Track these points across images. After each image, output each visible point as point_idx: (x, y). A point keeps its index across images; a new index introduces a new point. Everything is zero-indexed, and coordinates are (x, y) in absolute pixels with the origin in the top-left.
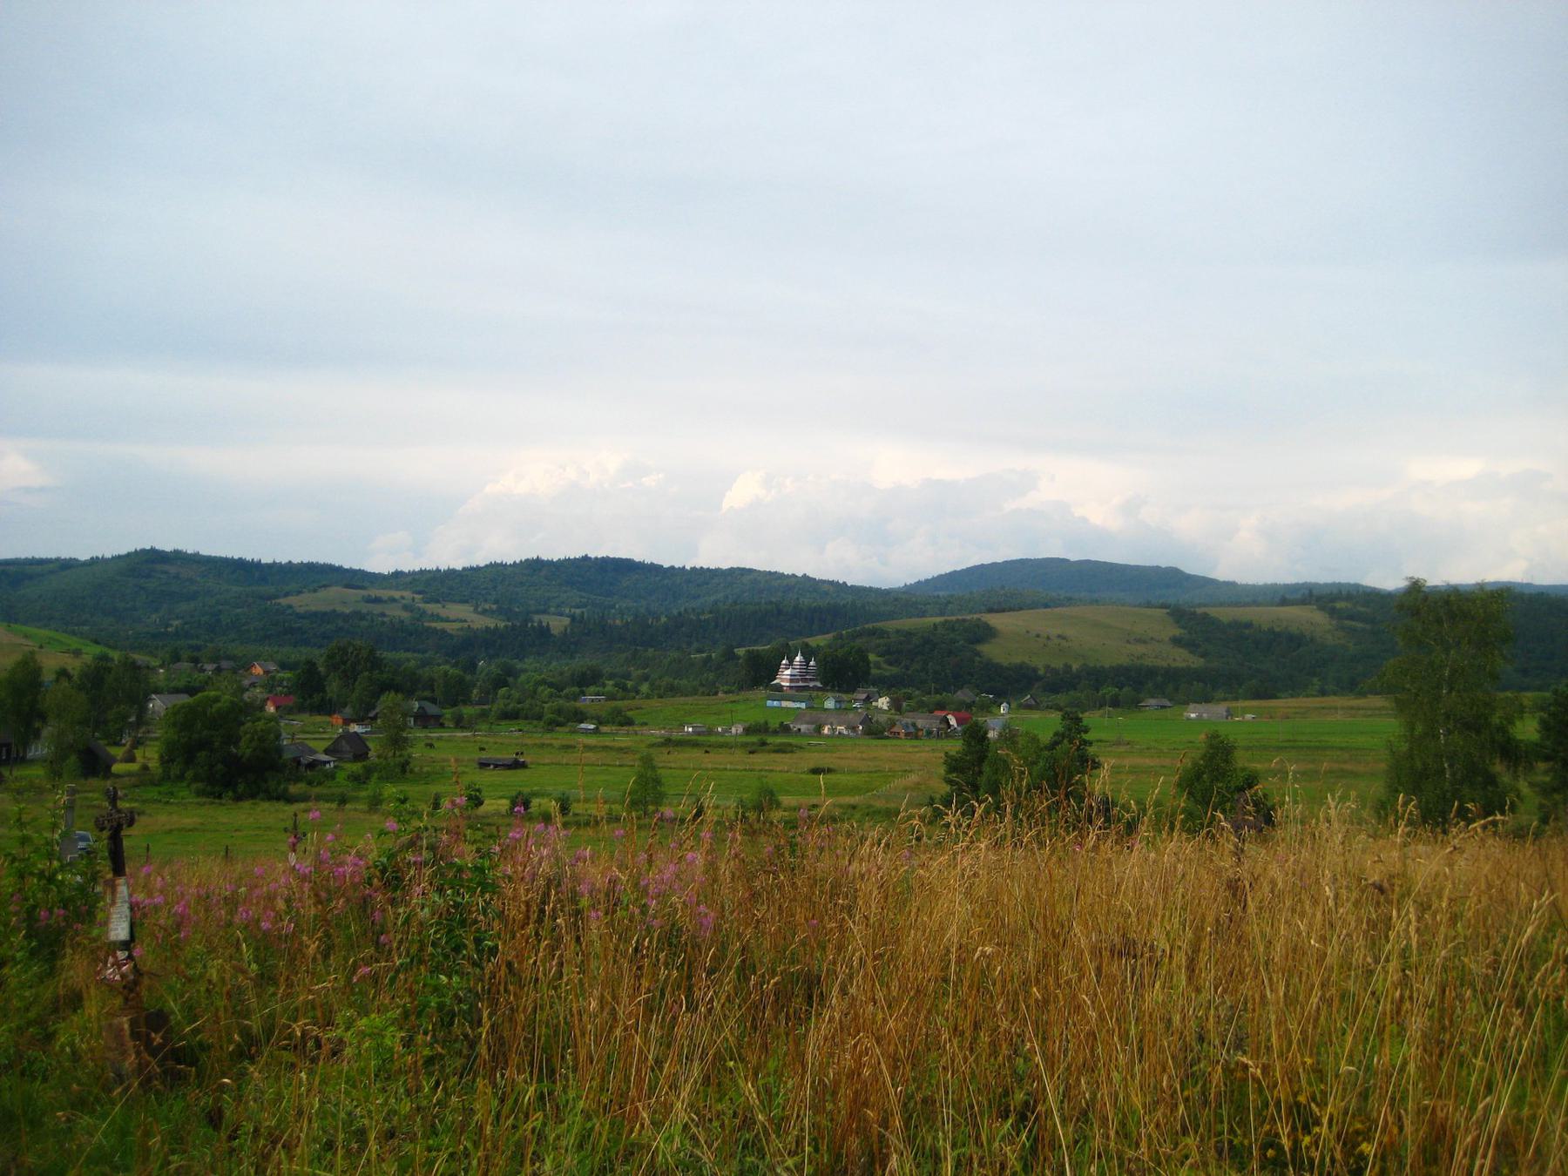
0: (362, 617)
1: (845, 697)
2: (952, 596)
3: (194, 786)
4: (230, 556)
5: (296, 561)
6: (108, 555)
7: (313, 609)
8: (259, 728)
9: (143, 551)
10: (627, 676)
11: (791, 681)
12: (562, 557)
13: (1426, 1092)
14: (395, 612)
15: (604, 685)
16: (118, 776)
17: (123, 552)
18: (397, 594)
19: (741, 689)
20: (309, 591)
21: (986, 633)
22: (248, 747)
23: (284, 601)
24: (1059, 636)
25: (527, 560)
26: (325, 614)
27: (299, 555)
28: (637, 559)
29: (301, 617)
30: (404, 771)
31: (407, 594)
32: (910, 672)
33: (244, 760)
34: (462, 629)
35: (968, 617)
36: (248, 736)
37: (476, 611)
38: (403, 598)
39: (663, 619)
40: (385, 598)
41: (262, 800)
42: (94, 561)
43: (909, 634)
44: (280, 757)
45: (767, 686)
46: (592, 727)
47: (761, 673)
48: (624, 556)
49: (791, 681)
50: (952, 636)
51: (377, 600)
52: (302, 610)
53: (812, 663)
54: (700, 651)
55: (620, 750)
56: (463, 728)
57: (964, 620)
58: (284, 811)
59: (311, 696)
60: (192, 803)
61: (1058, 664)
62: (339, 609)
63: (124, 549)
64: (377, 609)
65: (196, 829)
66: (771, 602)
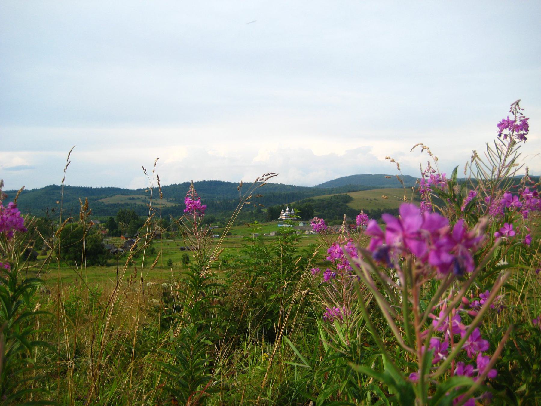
0: (127, 205)
1: (307, 222)
2: (333, 188)
3: (69, 262)
4: (81, 186)
5: (104, 187)
6: (39, 188)
7: (111, 203)
8: (94, 237)
9: (51, 186)
10: (223, 219)
11: (285, 217)
12: (196, 181)
13: (464, 353)
14: (139, 203)
15: (216, 223)
16: (39, 260)
17: (44, 187)
18: (140, 197)
19: (267, 221)
20: (109, 197)
21: (350, 199)
22: (90, 245)
23: (100, 201)
24: (375, 199)
25: (184, 183)
26: (115, 204)
27: (105, 185)
28: (222, 181)
29: (107, 206)
30: (152, 253)
31: (143, 196)
32: (324, 214)
33: (89, 250)
34: (163, 207)
35: (342, 194)
36: (90, 240)
37: (167, 201)
38: (142, 198)
39: (234, 200)
40: (136, 198)
41: (97, 266)
42: (34, 190)
43: (322, 201)
44: (103, 248)
45: (277, 220)
46: (218, 236)
47: (274, 215)
48: (218, 180)
49: (285, 217)
50: (337, 200)
51: (133, 199)
52: (107, 204)
53: (292, 211)
54: (248, 211)
55: (232, 243)
56: (169, 239)
57: (341, 195)
58: (106, 270)
59: (112, 230)
60: (67, 269)
61: (376, 209)
62: (120, 202)
63: (44, 186)
64: (133, 202)
65: (69, 278)
66: (271, 193)
